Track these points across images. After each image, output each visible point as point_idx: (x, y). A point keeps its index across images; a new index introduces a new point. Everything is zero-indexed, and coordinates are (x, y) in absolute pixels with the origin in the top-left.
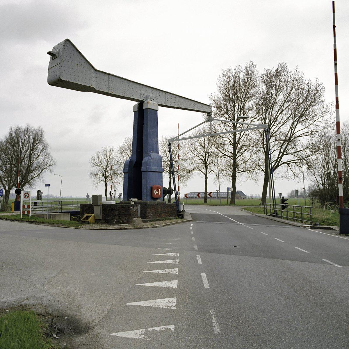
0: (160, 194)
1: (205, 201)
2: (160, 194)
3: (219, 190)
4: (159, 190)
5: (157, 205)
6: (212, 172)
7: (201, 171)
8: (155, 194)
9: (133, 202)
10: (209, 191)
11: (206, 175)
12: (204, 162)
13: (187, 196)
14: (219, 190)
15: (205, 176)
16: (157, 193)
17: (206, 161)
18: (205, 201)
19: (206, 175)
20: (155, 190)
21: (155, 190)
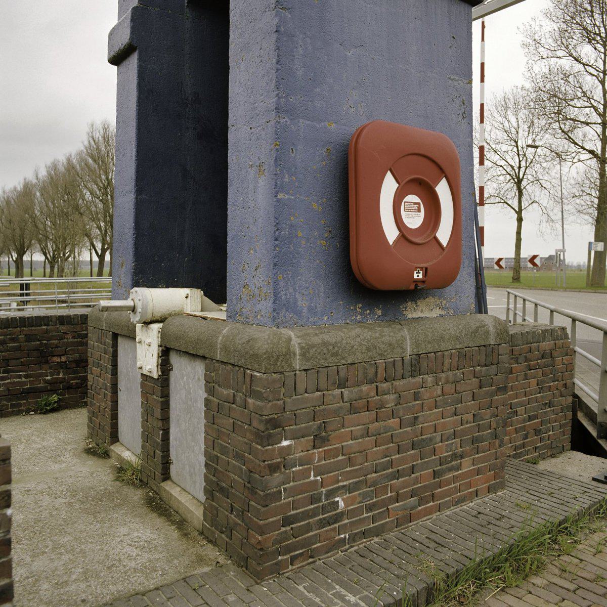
0: (444, 234)
1: (516, 279)
2: (444, 234)
3: (562, 248)
4: (443, 189)
5: (416, 366)
6: (535, 205)
7: (505, 202)
8: (391, 233)
9: (147, 323)
10: (525, 253)
11: (519, 212)
12: (514, 179)
13: (535, 261)
14: (562, 248)
15: (516, 215)
16: (414, 220)
17: (521, 176)
18: (516, 279)
19: (519, 212)
20: (389, 186)
21: (389, 186)
